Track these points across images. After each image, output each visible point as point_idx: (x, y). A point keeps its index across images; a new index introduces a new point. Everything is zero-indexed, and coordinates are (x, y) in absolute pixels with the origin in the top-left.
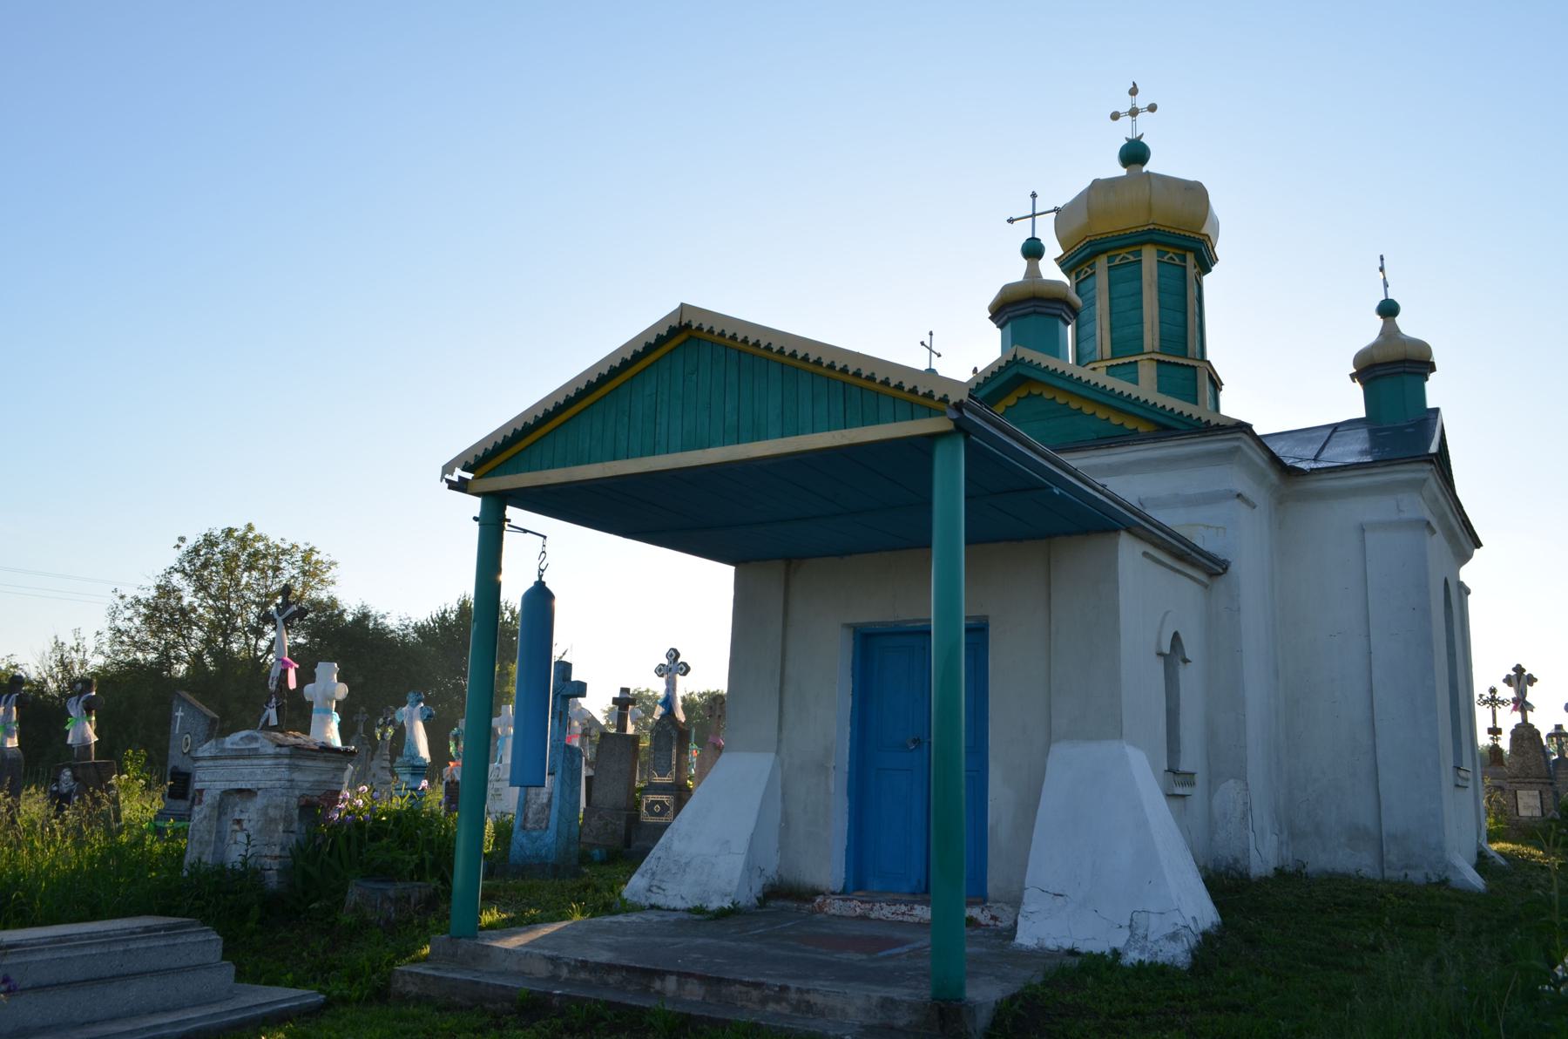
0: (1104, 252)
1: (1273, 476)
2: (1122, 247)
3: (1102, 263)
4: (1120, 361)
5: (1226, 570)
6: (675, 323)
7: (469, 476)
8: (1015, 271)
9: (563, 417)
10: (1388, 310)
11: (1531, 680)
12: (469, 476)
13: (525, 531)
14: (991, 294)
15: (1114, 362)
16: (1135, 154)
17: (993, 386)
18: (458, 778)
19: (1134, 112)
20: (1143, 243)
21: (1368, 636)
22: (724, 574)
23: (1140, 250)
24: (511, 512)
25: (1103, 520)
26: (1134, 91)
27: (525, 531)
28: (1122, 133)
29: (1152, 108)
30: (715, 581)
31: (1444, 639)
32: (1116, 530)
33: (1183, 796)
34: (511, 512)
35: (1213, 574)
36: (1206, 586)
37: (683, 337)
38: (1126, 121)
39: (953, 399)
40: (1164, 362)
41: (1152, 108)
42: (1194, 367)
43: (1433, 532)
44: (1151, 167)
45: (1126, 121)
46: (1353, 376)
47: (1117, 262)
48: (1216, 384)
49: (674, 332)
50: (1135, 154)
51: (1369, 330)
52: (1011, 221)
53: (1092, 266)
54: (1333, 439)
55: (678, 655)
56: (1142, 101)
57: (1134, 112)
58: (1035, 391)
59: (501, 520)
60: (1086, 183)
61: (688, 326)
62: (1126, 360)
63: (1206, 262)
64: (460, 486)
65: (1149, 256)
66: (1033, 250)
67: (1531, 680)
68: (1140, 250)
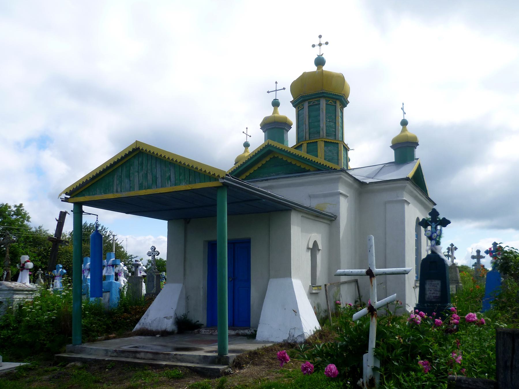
0: (307, 100)
1: (356, 185)
2: (312, 99)
3: (306, 105)
4: (312, 141)
5: (335, 219)
6: (134, 147)
7: (69, 197)
8: (269, 112)
9: (99, 178)
10: (404, 123)
11: (456, 249)
12: (69, 197)
13: (90, 214)
14: (260, 121)
15: (310, 142)
16: (320, 62)
17: (241, 169)
18: (163, 255)
19: (320, 45)
20: (320, 97)
21: (386, 238)
22: (166, 222)
23: (321, 97)
24: (85, 208)
25: (281, 210)
26: (320, 37)
27: (90, 214)
28: (315, 53)
29: (327, 43)
30: (162, 225)
31: (414, 238)
32: (290, 210)
33: (317, 293)
34: (85, 208)
35: (331, 221)
36: (329, 224)
37: (137, 152)
38: (317, 47)
39: (221, 176)
40: (326, 142)
41: (327, 43)
42: (338, 143)
43: (408, 203)
44: (325, 68)
45: (317, 47)
46: (391, 147)
47: (311, 104)
48: (347, 149)
49: (134, 150)
50: (320, 62)
51: (396, 130)
52: (268, 92)
53: (303, 105)
54: (382, 171)
55: (155, 249)
56: (323, 41)
57: (320, 45)
58: (276, 156)
59: (82, 212)
60: (300, 74)
61: (139, 148)
62: (314, 141)
63: (344, 103)
64: (66, 200)
65: (323, 103)
66: (276, 104)
67: (456, 249)
68: (321, 97)
